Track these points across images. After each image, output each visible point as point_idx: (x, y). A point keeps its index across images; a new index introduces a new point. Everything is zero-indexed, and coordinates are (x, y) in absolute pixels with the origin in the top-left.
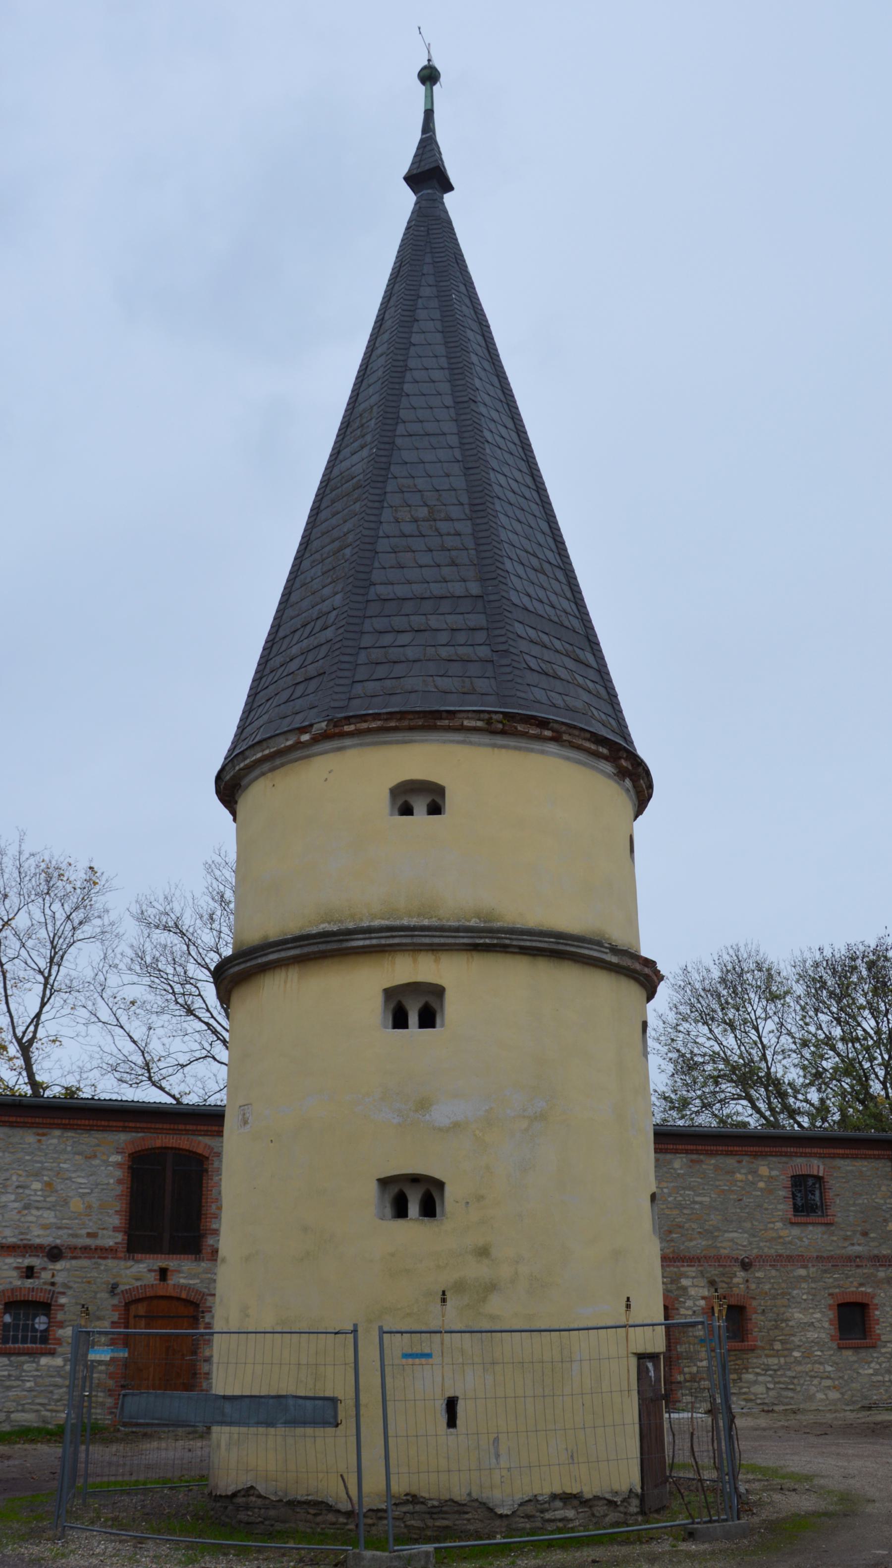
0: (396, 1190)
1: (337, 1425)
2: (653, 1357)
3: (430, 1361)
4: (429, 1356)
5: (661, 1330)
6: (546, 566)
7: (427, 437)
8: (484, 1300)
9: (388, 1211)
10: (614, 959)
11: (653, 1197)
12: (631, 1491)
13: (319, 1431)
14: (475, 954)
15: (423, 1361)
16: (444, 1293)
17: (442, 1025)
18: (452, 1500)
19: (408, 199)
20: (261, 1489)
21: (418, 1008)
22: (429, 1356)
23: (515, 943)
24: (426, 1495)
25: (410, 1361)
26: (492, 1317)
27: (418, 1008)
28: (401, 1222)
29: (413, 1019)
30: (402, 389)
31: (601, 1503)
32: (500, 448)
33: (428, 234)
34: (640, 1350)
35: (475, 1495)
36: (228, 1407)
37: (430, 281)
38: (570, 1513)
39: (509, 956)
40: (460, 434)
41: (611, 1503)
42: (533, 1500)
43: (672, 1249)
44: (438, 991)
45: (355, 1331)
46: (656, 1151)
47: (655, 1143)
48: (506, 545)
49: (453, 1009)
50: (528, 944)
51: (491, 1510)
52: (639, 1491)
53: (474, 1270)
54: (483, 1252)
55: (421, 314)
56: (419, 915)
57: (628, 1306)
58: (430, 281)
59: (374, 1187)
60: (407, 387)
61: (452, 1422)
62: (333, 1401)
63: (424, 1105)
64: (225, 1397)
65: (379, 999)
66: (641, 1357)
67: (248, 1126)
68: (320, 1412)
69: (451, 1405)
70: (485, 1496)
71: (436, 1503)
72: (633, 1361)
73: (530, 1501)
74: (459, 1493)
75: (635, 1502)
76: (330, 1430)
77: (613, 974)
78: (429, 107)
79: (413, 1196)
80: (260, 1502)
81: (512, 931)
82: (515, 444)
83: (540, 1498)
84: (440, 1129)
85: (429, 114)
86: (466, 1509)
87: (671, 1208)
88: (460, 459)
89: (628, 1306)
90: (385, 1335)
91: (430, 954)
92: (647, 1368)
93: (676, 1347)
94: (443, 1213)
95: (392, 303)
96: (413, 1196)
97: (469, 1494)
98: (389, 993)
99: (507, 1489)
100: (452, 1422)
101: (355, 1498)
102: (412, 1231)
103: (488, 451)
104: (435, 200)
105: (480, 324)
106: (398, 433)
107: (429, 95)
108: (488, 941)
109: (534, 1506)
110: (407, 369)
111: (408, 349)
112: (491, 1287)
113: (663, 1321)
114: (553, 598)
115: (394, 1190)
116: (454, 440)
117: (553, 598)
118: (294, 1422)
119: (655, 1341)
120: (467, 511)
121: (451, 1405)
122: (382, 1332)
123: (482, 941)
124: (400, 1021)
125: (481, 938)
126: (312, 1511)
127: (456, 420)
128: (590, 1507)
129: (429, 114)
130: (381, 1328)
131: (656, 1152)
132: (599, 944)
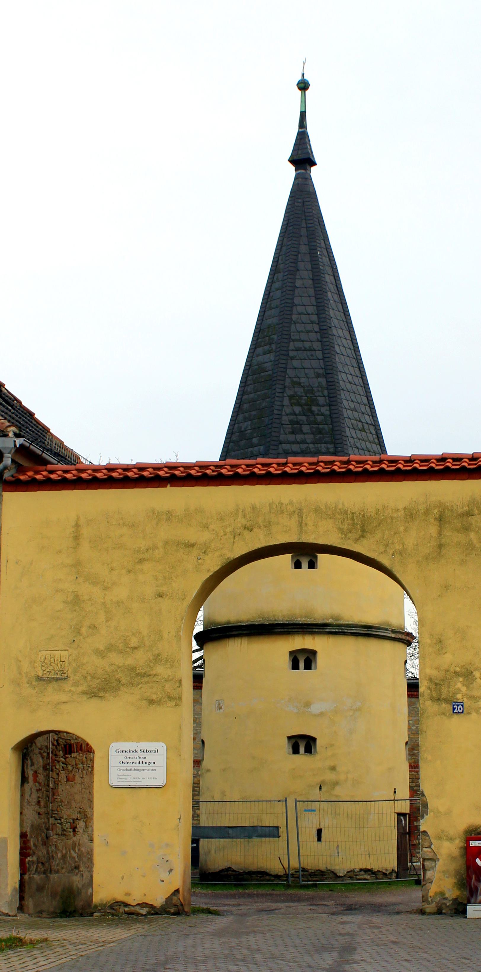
0: (294, 741)
1: (279, 837)
2: (404, 815)
3: (315, 813)
4: (314, 810)
5: (408, 802)
6: (366, 426)
7: (305, 352)
8: (333, 788)
9: (291, 750)
10: (393, 635)
11: (407, 743)
12: (393, 870)
13: (272, 839)
14: (330, 635)
15: (312, 812)
16: (321, 786)
17: (316, 668)
18: (319, 870)
19: (291, 171)
20: (234, 867)
21: (304, 660)
22: (314, 810)
23: (349, 631)
24: (308, 868)
25: (307, 812)
26: (337, 796)
27: (304, 660)
28: (296, 756)
29: (302, 665)
30: (292, 319)
31: (380, 873)
32: (343, 355)
33: (304, 205)
34: (400, 811)
35: (329, 868)
36: (230, 831)
37: (303, 236)
38: (367, 877)
39: (346, 636)
40: (323, 350)
41: (385, 874)
42: (353, 871)
43: (413, 760)
44: (314, 653)
45: (286, 800)
46: (409, 696)
47: (408, 691)
48: (346, 419)
49: (321, 660)
50: (355, 631)
51: (335, 874)
52: (396, 870)
53: (330, 776)
54: (333, 768)
55: (301, 265)
56: (305, 617)
57: (395, 792)
58: (303, 236)
59: (286, 740)
60: (294, 317)
61: (319, 839)
62: (277, 828)
63: (308, 704)
64: (229, 827)
65: (287, 655)
66: (399, 814)
67: (221, 711)
68: (273, 832)
69: (319, 832)
70: (333, 868)
71: (313, 871)
72: (396, 815)
73: (351, 871)
74: (323, 867)
75: (394, 875)
76: (277, 839)
77: (392, 641)
78: (303, 110)
79: (303, 744)
80: (234, 873)
81: (348, 626)
82: (350, 349)
83: (356, 870)
84: (315, 715)
85: (303, 115)
86: (325, 874)
87: (414, 734)
88: (323, 367)
89: (395, 792)
90: (298, 802)
91: (310, 635)
92: (401, 820)
93: (413, 823)
94: (316, 752)
95: (283, 252)
96: (303, 744)
97: (327, 868)
98: (291, 653)
99: (343, 864)
100: (319, 839)
101: (286, 866)
102: (302, 759)
103: (337, 360)
104: (306, 178)
105: (332, 268)
106: (290, 348)
107: (304, 100)
108: (337, 630)
109: (352, 874)
110: (293, 305)
111: (293, 291)
112: (336, 783)
113: (408, 798)
114: (369, 445)
115: (293, 741)
116: (319, 354)
117: (369, 445)
118: (261, 836)
119: (405, 808)
120: (328, 401)
121: (319, 832)
122: (296, 801)
123: (334, 631)
124: (295, 666)
125: (334, 629)
126: (259, 875)
127: (321, 341)
128: (376, 875)
129: (303, 115)
130: (296, 799)
131: (408, 697)
132: (387, 629)
